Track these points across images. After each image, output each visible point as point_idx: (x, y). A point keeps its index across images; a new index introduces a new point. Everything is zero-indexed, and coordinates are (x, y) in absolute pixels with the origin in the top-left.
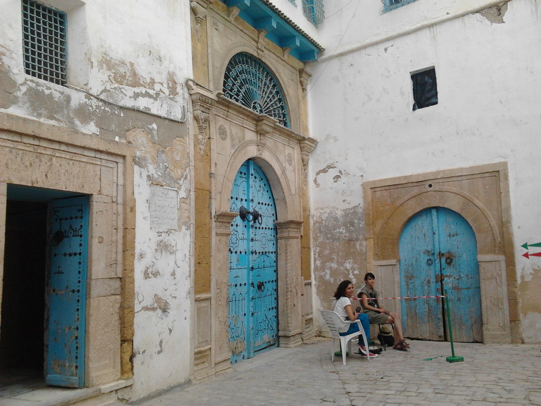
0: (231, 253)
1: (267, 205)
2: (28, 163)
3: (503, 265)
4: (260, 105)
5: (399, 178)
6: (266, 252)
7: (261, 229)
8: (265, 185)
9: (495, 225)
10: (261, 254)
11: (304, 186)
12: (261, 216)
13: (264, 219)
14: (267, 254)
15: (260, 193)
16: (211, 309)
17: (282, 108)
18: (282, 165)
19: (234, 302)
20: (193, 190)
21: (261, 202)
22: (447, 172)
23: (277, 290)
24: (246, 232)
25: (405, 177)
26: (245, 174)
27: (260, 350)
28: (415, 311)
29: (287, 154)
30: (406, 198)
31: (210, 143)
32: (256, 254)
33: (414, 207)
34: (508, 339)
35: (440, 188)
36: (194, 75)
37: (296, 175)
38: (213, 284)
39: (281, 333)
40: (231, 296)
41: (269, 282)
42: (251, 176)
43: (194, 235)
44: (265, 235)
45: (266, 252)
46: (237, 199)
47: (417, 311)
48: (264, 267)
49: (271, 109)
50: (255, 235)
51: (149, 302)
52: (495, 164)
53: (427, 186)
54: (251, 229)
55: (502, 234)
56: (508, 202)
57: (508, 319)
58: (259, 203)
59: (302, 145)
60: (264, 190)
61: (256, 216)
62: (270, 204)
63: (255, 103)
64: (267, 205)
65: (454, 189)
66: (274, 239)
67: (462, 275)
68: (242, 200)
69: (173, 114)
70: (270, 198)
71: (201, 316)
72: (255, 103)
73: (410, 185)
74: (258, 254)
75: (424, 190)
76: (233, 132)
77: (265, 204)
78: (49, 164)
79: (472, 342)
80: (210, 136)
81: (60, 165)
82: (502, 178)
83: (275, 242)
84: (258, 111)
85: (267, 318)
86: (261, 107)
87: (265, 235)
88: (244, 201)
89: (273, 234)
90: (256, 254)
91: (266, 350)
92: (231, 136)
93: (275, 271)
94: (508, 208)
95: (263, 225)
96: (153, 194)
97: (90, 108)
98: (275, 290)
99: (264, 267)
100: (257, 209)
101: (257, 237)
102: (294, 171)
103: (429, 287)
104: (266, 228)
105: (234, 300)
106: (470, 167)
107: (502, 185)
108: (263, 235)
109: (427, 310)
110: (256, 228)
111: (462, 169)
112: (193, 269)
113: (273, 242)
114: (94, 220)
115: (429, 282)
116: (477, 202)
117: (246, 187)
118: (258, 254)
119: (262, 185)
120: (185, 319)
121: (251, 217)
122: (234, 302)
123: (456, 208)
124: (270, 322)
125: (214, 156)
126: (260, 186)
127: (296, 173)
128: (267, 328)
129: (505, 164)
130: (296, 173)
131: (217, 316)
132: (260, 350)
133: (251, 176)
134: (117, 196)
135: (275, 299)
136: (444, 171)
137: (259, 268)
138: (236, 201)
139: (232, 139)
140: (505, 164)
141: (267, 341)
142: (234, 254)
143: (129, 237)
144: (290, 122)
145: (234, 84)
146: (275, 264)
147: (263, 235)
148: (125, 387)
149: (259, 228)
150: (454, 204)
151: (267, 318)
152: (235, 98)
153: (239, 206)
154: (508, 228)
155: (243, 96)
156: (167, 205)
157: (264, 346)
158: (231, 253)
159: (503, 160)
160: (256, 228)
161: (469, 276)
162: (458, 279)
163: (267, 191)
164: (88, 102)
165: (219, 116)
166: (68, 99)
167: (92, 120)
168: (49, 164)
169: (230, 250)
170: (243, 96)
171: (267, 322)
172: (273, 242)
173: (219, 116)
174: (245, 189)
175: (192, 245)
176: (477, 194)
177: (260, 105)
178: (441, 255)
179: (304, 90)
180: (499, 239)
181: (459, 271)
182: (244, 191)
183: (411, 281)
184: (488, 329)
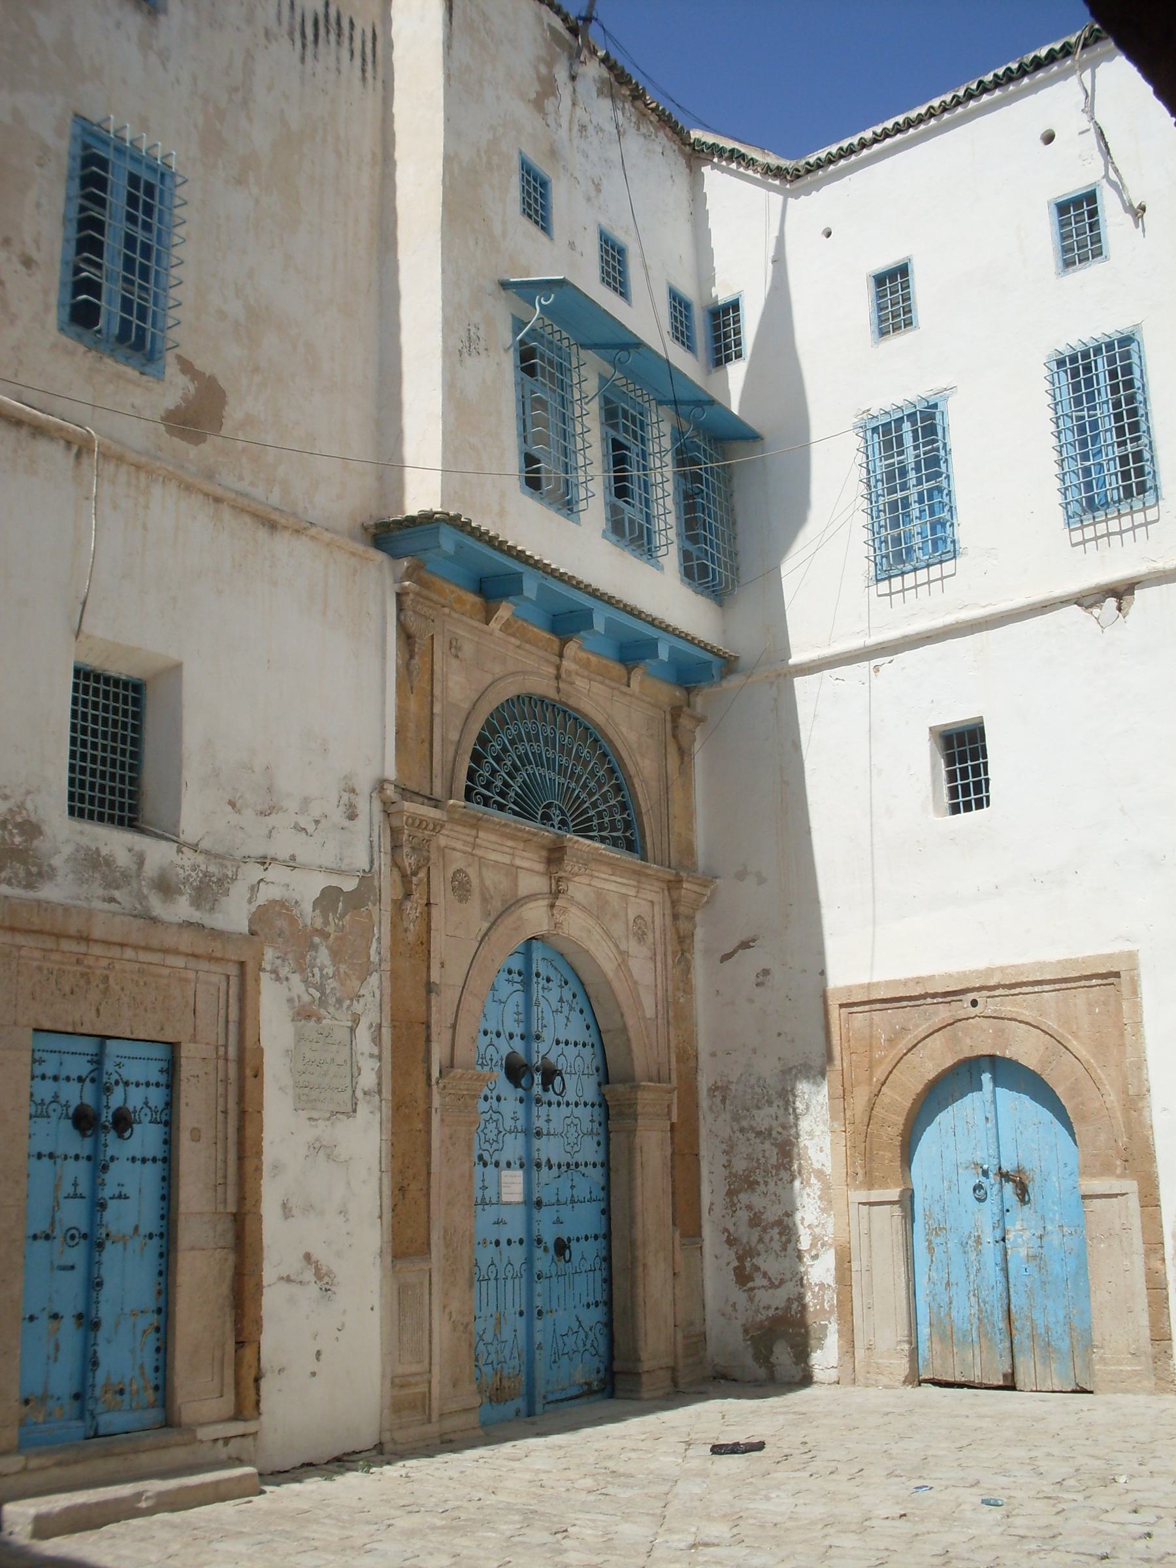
0: (485, 1165)
1: (580, 1046)
2: (67, 989)
3: (1134, 1202)
4: (560, 809)
5: (905, 983)
6: (577, 1165)
7: (563, 1107)
8: (574, 996)
9: (1116, 1104)
10: (564, 1168)
11: (680, 994)
12: (560, 1074)
13: (571, 1082)
14: (582, 1168)
15: (561, 1018)
16: (430, 1294)
17: (624, 807)
18: (617, 946)
19: (492, 1283)
20: (386, 1024)
21: (563, 1039)
22: (1009, 971)
23: (608, 1259)
24: (521, 1114)
25: (918, 981)
26: (520, 974)
27: (562, 1400)
28: (949, 1314)
29: (631, 917)
30: (922, 1031)
31: (429, 914)
32: (550, 1168)
33: (934, 1059)
34: (1146, 1383)
35: (995, 1011)
36: (399, 769)
37: (659, 969)
38: (435, 1236)
39: (617, 1366)
40: (484, 1267)
41: (587, 1238)
42: (535, 979)
43: (390, 1126)
44: (576, 1121)
45: (577, 1165)
46: (498, 1035)
47: (954, 1314)
48: (573, 1202)
49: (592, 813)
50: (548, 1121)
51: (293, 1264)
52: (1110, 957)
53: (967, 1004)
54: (535, 1109)
55: (1128, 1124)
56: (1140, 1050)
57: (1146, 1333)
58: (558, 1043)
59: (675, 895)
60: (571, 1009)
61: (550, 1075)
62: (589, 1041)
63: (549, 806)
64: (580, 1046)
65: (1026, 1014)
66: (601, 1130)
67: (1049, 1228)
68: (511, 1036)
69: (346, 861)
70: (588, 1027)
71: (404, 1304)
72: (549, 806)
73: (929, 1000)
74: (555, 1168)
75: (962, 1014)
76: (488, 883)
77: (576, 1044)
78: (101, 986)
79: (1073, 1392)
80: (429, 899)
81: (122, 989)
82: (1125, 989)
83: (601, 1138)
84: (556, 823)
85: (580, 1325)
86: (563, 813)
87: (576, 1121)
88: (517, 1039)
89: (597, 1118)
90: (550, 1168)
91: (578, 1401)
92: (482, 894)
93: (603, 1212)
94: (1140, 1065)
95: (570, 1096)
96: (300, 1038)
97: (181, 871)
98: (604, 1259)
99: (573, 1202)
100: (552, 1058)
101: (552, 1125)
102: (653, 959)
103: (979, 1253)
104: (577, 1104)
105: (493, 1276)
106: (1059, 962)
107: (1125, 1006)
108: (568, 1121)
109: (974, 1311)
110: (550, 1104)
111: (1042, 966)
112: (387, 1202)
113: (596, 1138)
114: (183, 1094)
115: (978, 1240)
116: (1074, 1044)
117: (521, 1003)
118: (555, 1168)
119: (567, 996)
120: (372, 1309)
121: (538, 1078)
122: (492, 1283)
123: (1030, 1061)
124: (591, 1337)
125: (439, 943)
126: (561, 1000)
127: (659, 964)
128: (582, 1350)
129: (1131, 956)
130: (659, 964)
131: (447, 1311)
132: (562, 1400)
133: (535, 979)
134: (226, 1046)
135: (605, 1281)
136: (1002, 969)
137: (558, 1203)
138: (495, 1040)
139: (485, 900)
140: (1131, 956)
141: (583, 1381)
142: (491, 1167)
143: (250, 1131)
144: (643, 836)
145: (494, 772)
146: (602, 1194)
147: (568, 1121)
148: (243, 1436)
149: (559, 1104)
150: (1025, 1049)
151: (580, 1325)
152: (495, 802)
153: (505, 1050)
154: (1139, 1111)
155: (517, 794)
156: (329, 1060)
157: (574, 1391)
158: (485, 1165)
159: (1127, 947)
160: (550, 1104)
161: (1065, 1229)
162: (1041, 1237)
163: (581, 1012)
164: (177, 859)
165: (454, 849)
166: (141, 860)
167: (181, 893)
168: (101, 986)
169: (481, 1157)
170: (517, 794)
171: (582, 1335)
172: (596, 1138)
173: (454, 849)
174: (521, 1009)
175: (386, 1147)
176: (1074, 1028)
177: (560, 809)
178: (1004, 1176)
179: (684, 754)
180: (1123, 1140)
181: (1043, 1218)
182: (518, 1013)
183: (938, 1240)
184: (1102, 1359)
